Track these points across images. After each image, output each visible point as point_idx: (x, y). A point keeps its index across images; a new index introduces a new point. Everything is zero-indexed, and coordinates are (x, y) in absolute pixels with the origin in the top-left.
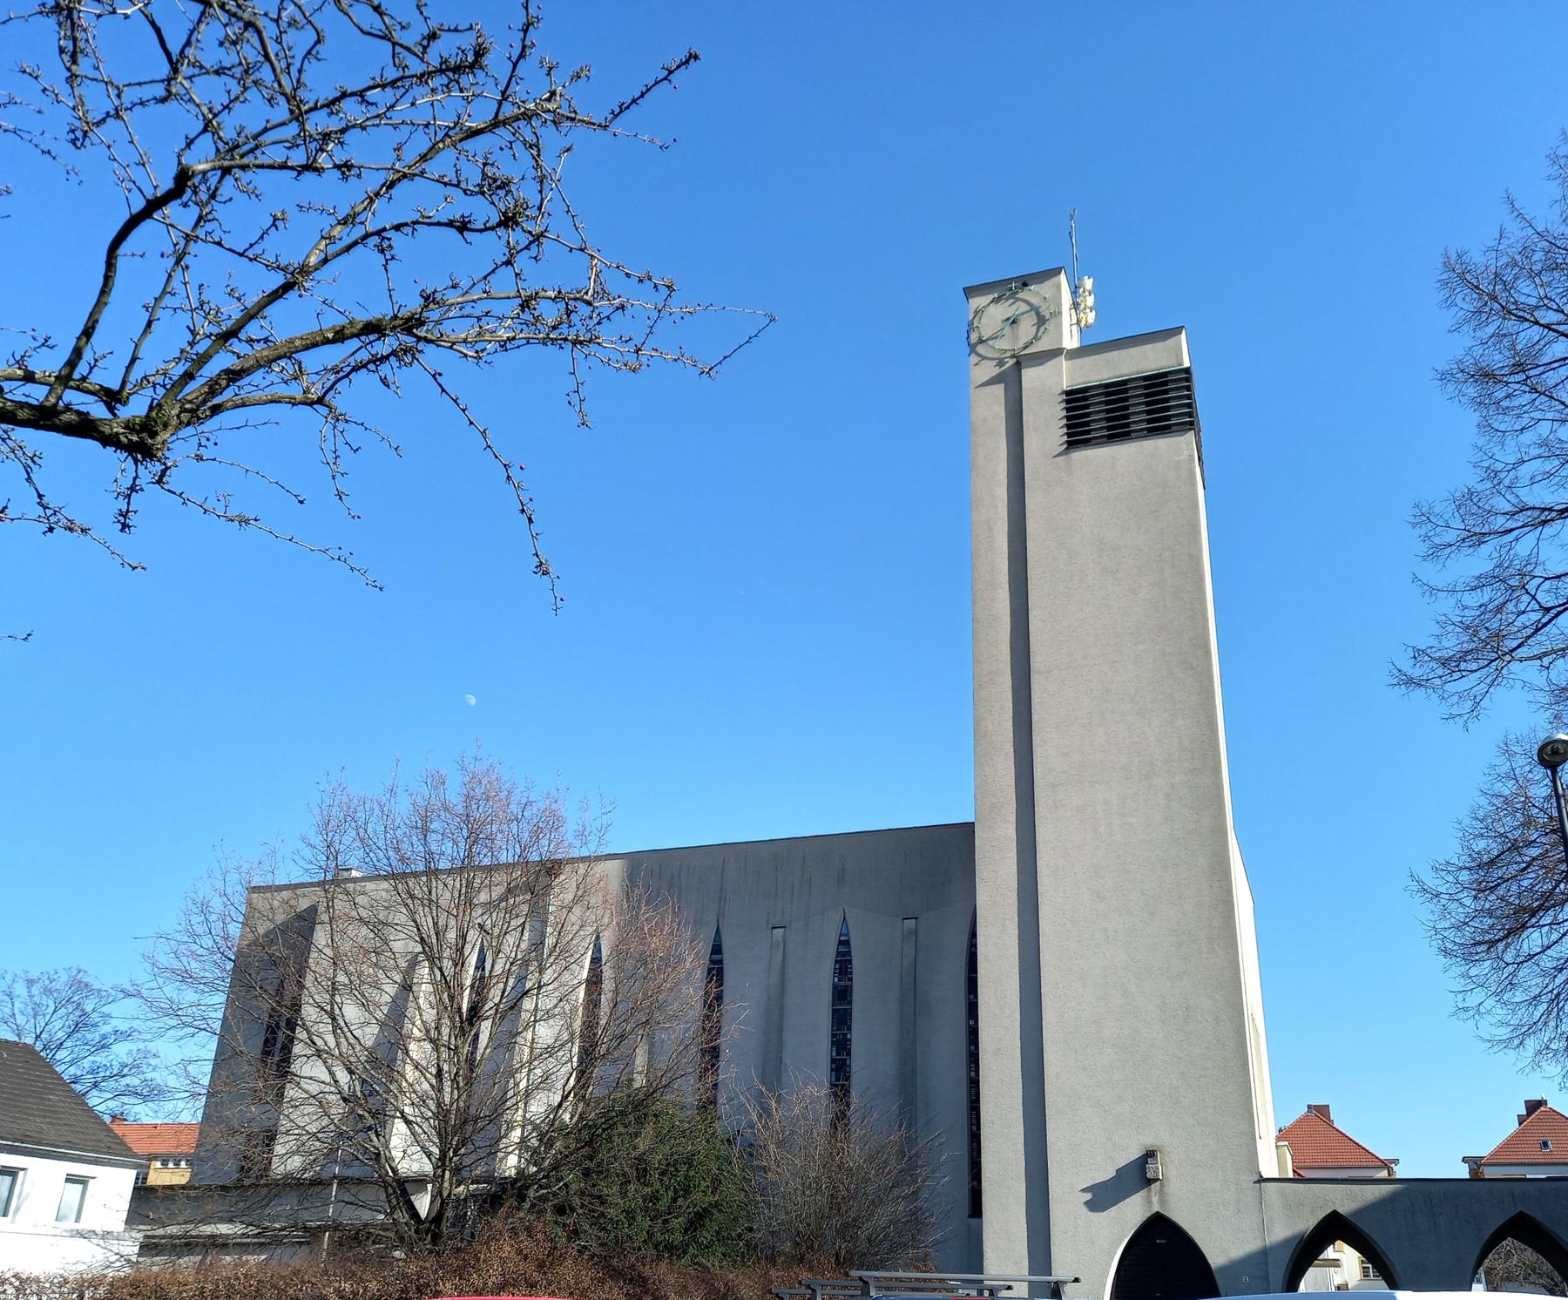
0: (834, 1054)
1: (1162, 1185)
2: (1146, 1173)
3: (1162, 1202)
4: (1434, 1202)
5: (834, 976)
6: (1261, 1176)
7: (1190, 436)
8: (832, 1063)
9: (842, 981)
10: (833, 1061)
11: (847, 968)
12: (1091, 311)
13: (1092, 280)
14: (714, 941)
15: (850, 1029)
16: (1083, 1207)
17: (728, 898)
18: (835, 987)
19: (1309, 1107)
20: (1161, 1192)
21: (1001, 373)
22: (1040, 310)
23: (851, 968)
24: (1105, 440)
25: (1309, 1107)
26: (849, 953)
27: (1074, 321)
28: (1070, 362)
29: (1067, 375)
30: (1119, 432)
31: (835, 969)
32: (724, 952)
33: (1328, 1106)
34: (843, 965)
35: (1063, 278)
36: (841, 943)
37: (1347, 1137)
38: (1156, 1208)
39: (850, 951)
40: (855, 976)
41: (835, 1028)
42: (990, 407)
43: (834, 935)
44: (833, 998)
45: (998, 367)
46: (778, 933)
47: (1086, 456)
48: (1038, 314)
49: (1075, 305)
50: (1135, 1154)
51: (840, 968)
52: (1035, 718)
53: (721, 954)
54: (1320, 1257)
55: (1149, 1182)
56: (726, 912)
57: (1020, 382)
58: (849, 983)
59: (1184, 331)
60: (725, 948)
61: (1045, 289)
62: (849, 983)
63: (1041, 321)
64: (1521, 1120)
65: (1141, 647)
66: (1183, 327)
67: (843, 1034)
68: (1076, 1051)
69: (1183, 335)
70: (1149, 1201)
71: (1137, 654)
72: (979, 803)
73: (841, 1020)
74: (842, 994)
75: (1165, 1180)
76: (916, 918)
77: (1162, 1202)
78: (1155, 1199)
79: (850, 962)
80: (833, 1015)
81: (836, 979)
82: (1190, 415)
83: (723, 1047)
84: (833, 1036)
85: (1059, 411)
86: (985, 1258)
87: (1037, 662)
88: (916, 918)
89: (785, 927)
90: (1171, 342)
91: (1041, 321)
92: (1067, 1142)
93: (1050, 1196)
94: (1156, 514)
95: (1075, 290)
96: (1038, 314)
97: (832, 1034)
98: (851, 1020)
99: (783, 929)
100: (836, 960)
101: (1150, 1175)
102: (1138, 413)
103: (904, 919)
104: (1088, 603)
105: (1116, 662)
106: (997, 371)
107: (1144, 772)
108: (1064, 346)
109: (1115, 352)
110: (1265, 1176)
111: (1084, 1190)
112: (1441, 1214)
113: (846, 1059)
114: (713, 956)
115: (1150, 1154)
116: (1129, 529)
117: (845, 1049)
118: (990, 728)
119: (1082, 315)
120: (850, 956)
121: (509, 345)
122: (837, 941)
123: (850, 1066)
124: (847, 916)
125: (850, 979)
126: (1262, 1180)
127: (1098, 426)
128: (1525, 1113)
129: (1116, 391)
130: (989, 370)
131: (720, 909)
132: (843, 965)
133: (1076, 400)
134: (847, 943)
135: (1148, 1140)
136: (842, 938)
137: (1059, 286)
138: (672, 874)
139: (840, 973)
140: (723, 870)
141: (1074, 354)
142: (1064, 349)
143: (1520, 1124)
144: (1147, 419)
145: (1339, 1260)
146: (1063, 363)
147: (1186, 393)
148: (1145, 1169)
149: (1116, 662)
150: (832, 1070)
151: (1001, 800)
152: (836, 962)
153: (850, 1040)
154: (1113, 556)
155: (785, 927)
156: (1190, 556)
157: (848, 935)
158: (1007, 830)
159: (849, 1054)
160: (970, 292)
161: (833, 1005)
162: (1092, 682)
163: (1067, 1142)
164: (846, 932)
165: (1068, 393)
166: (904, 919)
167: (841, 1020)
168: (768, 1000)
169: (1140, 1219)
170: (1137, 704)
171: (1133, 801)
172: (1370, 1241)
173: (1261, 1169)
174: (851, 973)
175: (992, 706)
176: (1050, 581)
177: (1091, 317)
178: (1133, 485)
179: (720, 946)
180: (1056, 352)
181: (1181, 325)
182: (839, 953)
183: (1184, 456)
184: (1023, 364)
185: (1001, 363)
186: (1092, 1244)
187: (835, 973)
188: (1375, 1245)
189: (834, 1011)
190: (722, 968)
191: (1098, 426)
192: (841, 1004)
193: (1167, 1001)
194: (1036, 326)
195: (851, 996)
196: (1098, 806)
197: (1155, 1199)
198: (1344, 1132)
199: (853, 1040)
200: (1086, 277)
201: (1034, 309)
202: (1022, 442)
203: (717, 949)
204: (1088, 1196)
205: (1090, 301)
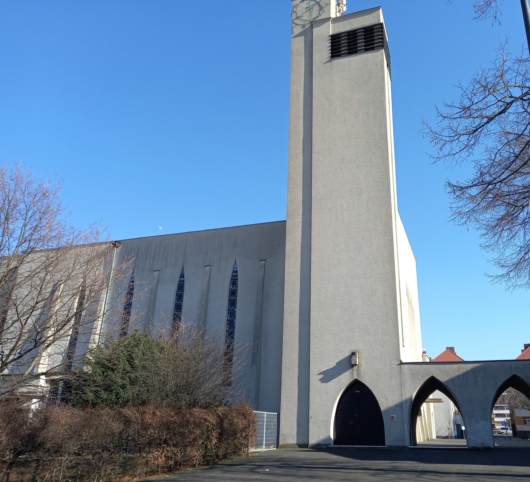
0: (229, 317)
1: (358, 367)
2: (351, 362)
3: (358, 374)
4: (476, 371)
5: (230, 286)
6: (401, 362)
7: (383, 51)
8: (227, 321)
9: (233, 287)
11: (235, 282)
12: (344, 6)
14: (181, 273)
16: (319, 382)
17: (187, 254)
18: (230, 290)
20: (358, 370)
22: (320, 3)
23: (237, 282)
26: (237, 276)
27: (338, 11)
28: (333, 25)
29: (332, 29)
30: (353, 51)
31: (231, 282)
33: (454, 347)
34: (234, 282)
36: (234, 272)
37: (460, 358)
38: (355, 377)
39: (237, 275)
41: (229, 307)
42: (299, 44)
43: (231, 268)
44: (229, 295)
45: (302, 28)
47: (339, 62)
50: (348, 354)
51: (233, 282)
52: (313, 172)
53: (184, 278)
55: (353, 366)
57: (312, 33)
58: (236, 288)
60: (185, 275)
63: (321, 8)
64: (522, 351)
65: (359, 140)
66: (381, 6)
69: (381, 10)
70: (352, 374)
72: (289, 208)
73: (232, 303)
74: (233, 293)
75: (359, 365)
76: (265, 260)
77: (358, 374)
78: (355, 373)
79: (237, 279)
81: (231, 287)
82: (383, 42)
84: (229, 310)
85: (328, 44)
89: (210, 266)
90: (375, 13)
91: (321, 8)
92: (319, 350)
93: (310, 373)
94: (367, 84)
96: (319, 5)
97: (228, 309)
98: (236, 303)
99: (209, 267)
100: (231, 279)
101: (353, 363)
105: (348, 147)
106: (302, 30)
107: (358, 192)
108: (331, 16)
109: (352, 19)
111: (319, 374)
112: (479, 376)
114: (180, 279)
116: (355, 91)
117: (233, 315)
118: (294, 177)
120: (237, 277)
121: (410, 301)
122: (232, 271)
124: (236, 261)
125: (237, 287)
126: (402, 363)
127: (344, 48)
128: (524, 349)
129: (352, 35)
130: (297, 30)
131: (184, 259)
132: (234, 282)
133: (335, 39)
134: (236, 272)
135: (353, 348)
140: (186, 243)
141: (336, 20)
142: (331, 17)
143: (522, 353)
145: (441, 399)
151: (298, 207)
152: (231, 279)
153: (236, 312)
155: (210, 266)
156: (381, 101)
157: (236, 268)
158: (299, 219)
159: (235, 317)
161: (229, 297)
163: (319, 350)
164: (236, 267)
165: (332, 36)
167: (232, 303)
168: (202, 296)
170: (356, 164)
171: (353, 205)
172: (448, 389)
174: (237, 284)
175: (296, 168)
176: (322, 114)
177: (345, 9)
180: (328, 19)
181: (379, 6)
183: (379, 60)
184: (314, 25)
185: (303, 26)
187: (230, 284)
188: (450, 391)
189: (230, 300)
190: (184, 283)
191: (344, 48)
192: (232, 297)
194: (319, 11)
196: (338, 207)
197: (355, 373)
198: (459, 357)
202: (312, 58)
203: (182, 276)
204: (322, 376)
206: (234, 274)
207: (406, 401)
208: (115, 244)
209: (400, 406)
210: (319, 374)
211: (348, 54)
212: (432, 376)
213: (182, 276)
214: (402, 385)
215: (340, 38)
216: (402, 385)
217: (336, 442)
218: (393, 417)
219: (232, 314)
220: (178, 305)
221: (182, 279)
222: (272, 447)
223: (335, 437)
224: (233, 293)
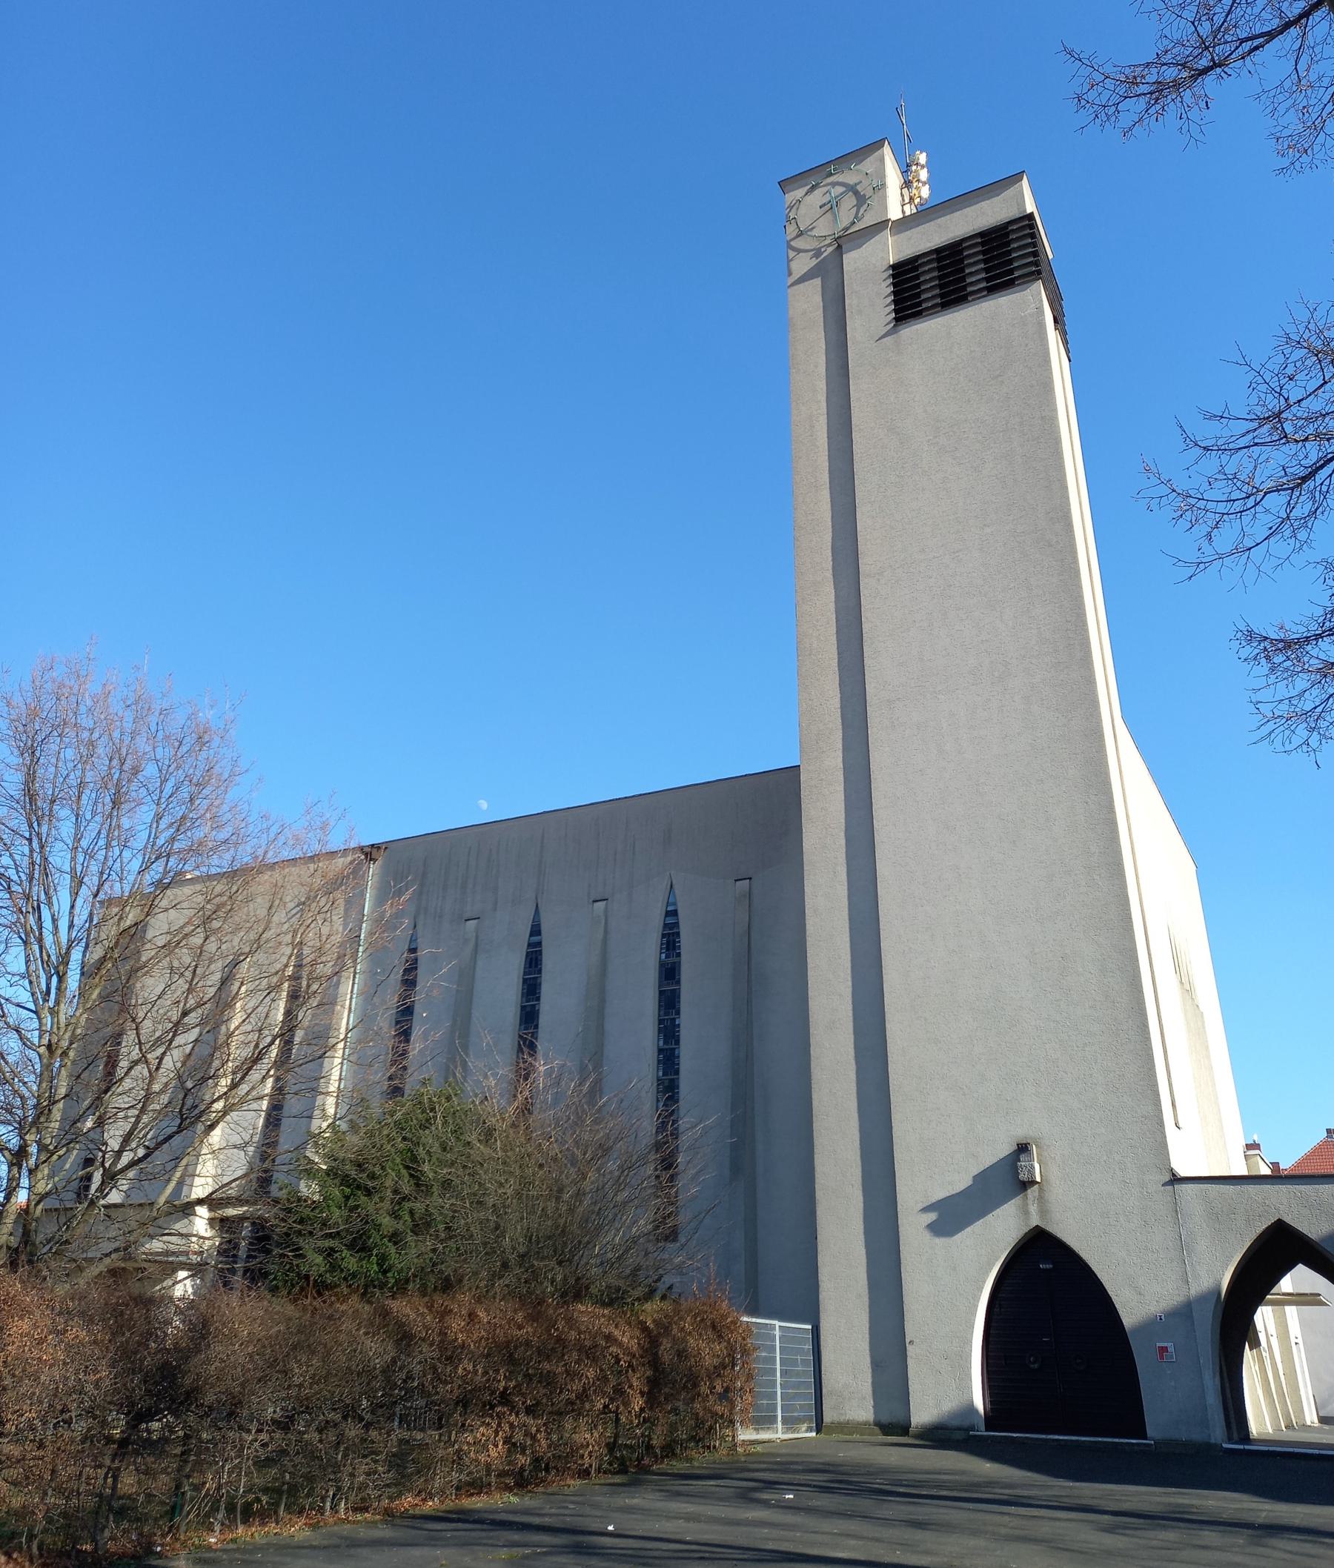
1: (1041, 1190)
5: (661, 953)
6: (1174, 1175)
10: (660, 1051)
13: (924, 154)
15: (678, 1013)
18: (662, 964)
19: (1329, 1131)
20: (1041, 1199)
21: (820, 262)
23: (679, 942)
24: (985, 293)
25: (1329, 1131)
26: (676, 925)
28: (896, 237)
29: (893, 249)
30: (953, 296)
32: (543, 932)
34: (670, 940)
35: (887, 150)
36: (668, 914)
38: (1035, 1221)
39: (678, 923)
40: (683, 951)
41: (662, 1013)
44: (660, 977)
46: (601, 905)
48: (856, 193)
49: (907, 184)
50: (1005, 1149)
51: (668, 942)
54: (1272, 1292)
55: (1025, 1185)
56: (545, 888)
59: (1025, 177)
61: (868, 165)
62: (676, 959)
63: (861, 200)
65: (988, 530)
67: (671, 1019)
68: (926, 1019)
69: (1025, 182)
71: (984, 538)
73: (669, 1002)
74: (669, 973)
75: (1044, 1183)
76: (750, 879)
77: (1043, 1212)
78: (1033, 1209)
79: (678, 934)
80: (660, 998)
81: (663, 956)
83: (417, 1008)
84: (660, 1022)
85: (886, 288)
86: (820, 1289)
87: (866, 564)
88: (750, 879)
91: (861, 200)
94: (1000, 379)
95: (906, 169)
96: (856, 193)
98: (679, 1002)
101: (1023, 1176)
102: (975, 273)
103: (736, 880)
104: (923, 490)
106: (814, 262)
110: (1183, 1172)
113: (674, 1049)
114: (532, 938)
115: (1023, 1148)
117: (673, 1036)
119: (914, 191)
120: (678, 927)
123: (678, 1057)
126: (1176, 1180)
127: (929, 294)
129: (950, 256)
132: (670, 940)
134: (674, 913)
136: (669, 909)
137: (882, 160)
138: (491, 850)
139: (668, 949)
141: (905, 223)
144: (985, 278)
146: (888, 239)
147: (1031, 250)
148: (1017, 1169)
149: (961, 550)
150: (659, 1062)
152: (663, 936)
154: (951, 433)
157: (675, 904)
158: (833, 760)
159: (677, 1042)
160: (785, 185)
161: (660, 986)
162: (931, 578)
165: (894, 267)
166: (736, 880)
167: (669, 1002)
169: (1014, 1236)
173: (1173, 1165)
177: (925, 192)
178: (971, 352)
179: (539, 925)
180: (883, 225)
182: (665, 925)
183: (1031, 310)
186: (954, 1269)
187: (661, 949)
189: (661, 993)
190: (541, 951)
191: (929, 294)
192: (668, 984)
193: (1037, 950)
194: (855, 208)
195: (679, 974)
197: (1033, 1209)
199: (681, 1026)
200: (918, 152)
201: (852, 189)
203: (536, 930)
204: (932, 1216)
205: (924, 175)
206: (670, 920)
207: (1202, 1298)
208: (370, 853)
209: (1184, 1313)
210: (926, 1209)
211: (942, 307)
212: (1279, 1220)
213: (536, 930)
214: (1182, 1247)
215: (916, 268)
216: (1182, 1247)
217: (992, 1420)
218: (1164, 1349)
219: (669, 1031)
220: (528, 1009)
221: (535, 939)
222: (804, 1427)
223: (989, 1406)
224: (669, 973)
